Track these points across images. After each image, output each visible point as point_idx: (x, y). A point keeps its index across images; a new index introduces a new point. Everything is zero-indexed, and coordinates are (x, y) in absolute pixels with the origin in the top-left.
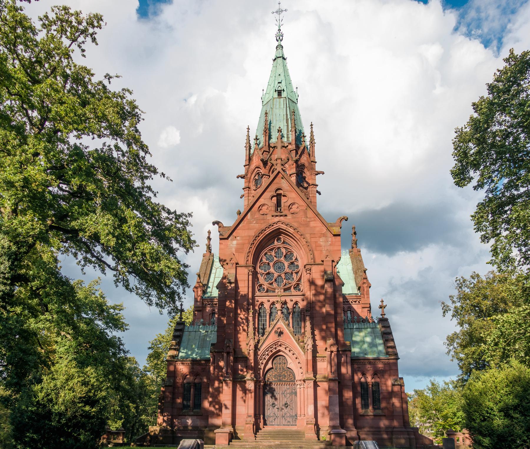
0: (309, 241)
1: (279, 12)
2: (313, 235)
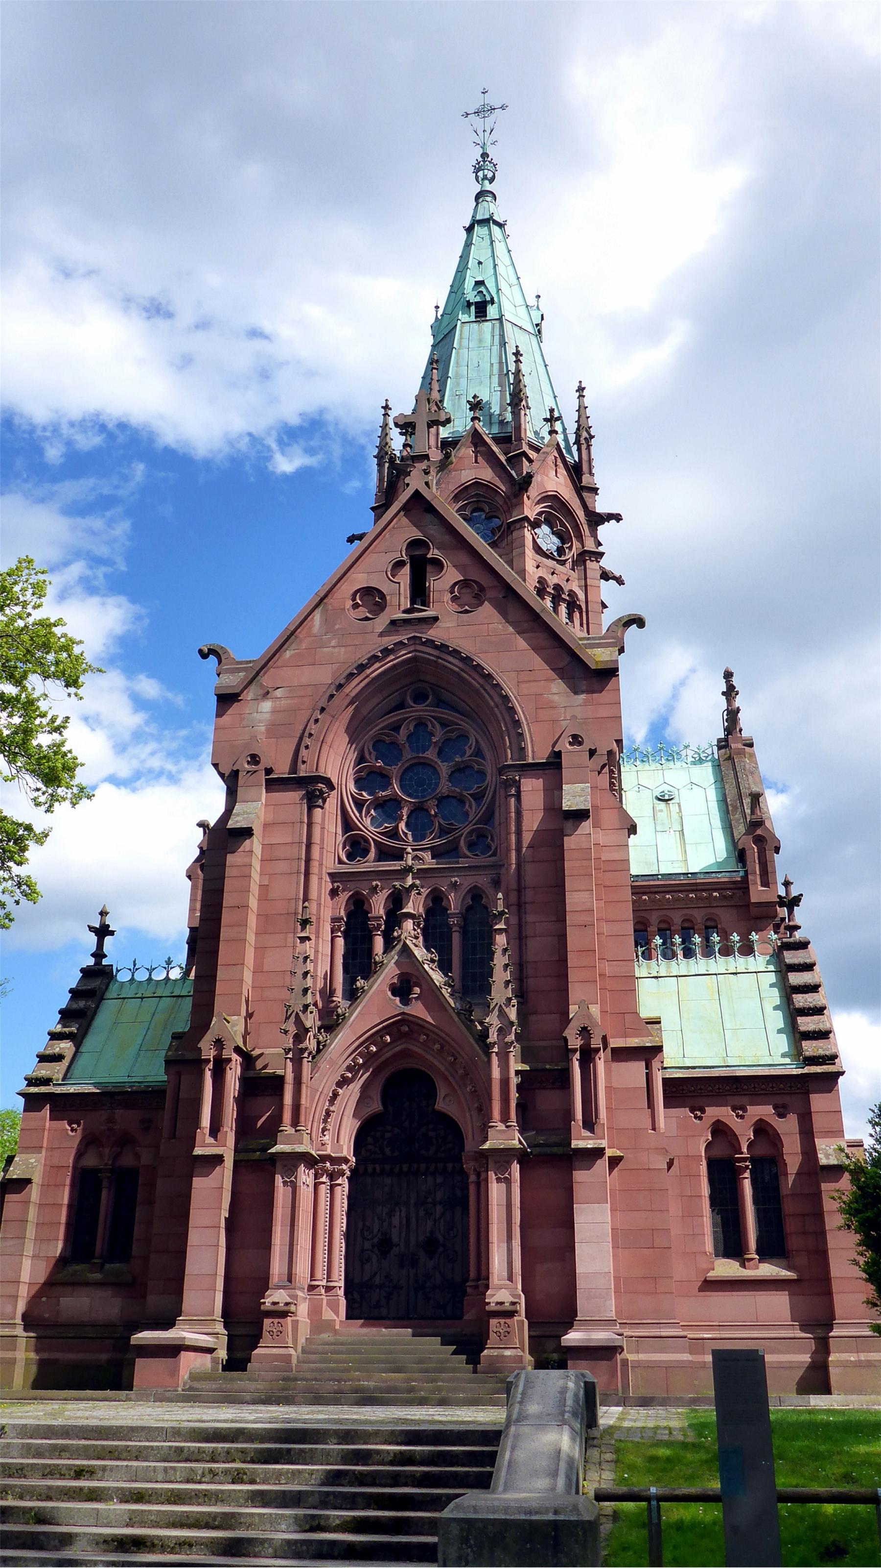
1: (484, 111)
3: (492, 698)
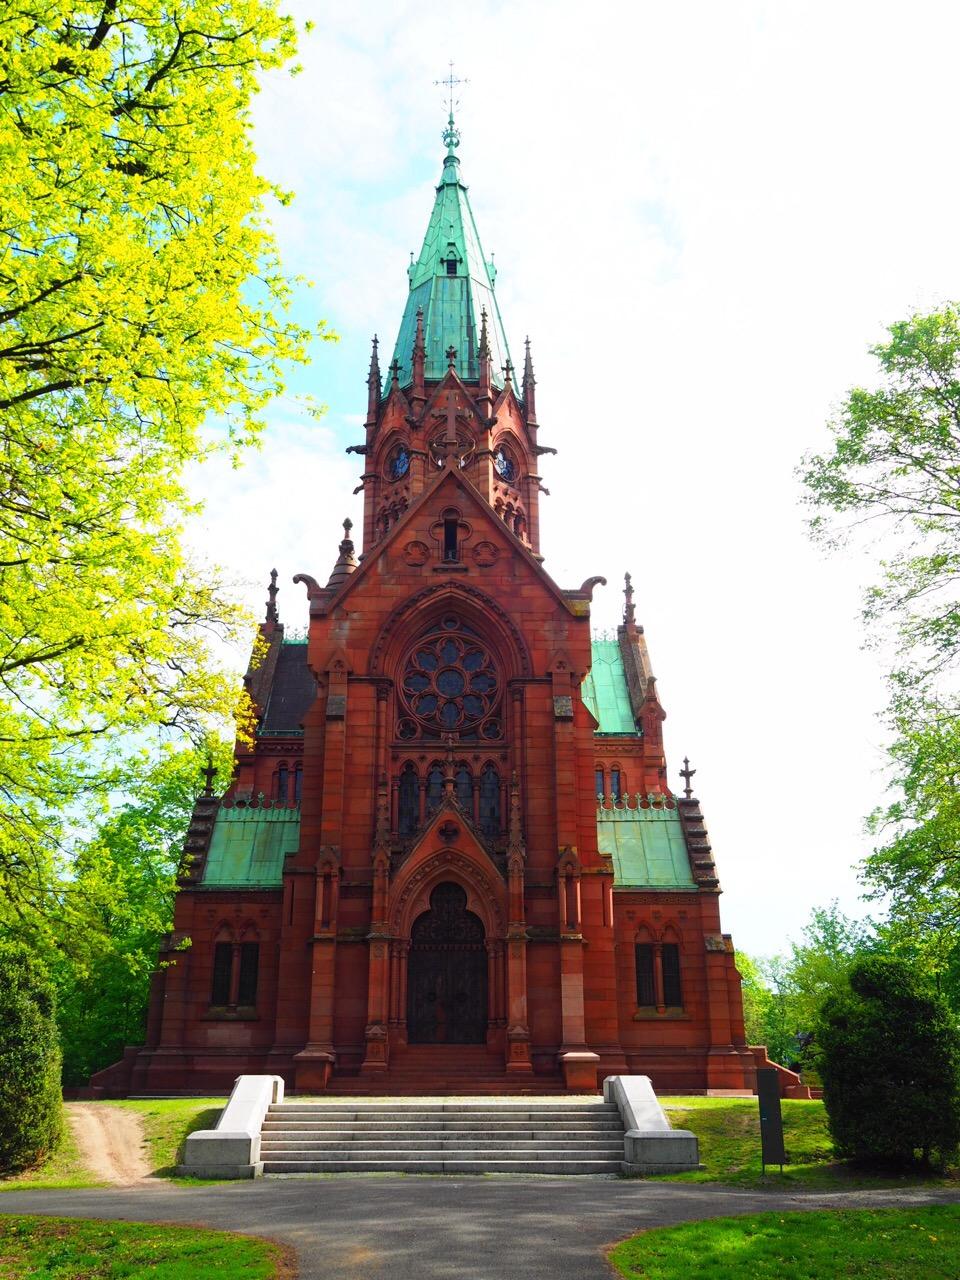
1: (451, 81)
3: (504, 630)
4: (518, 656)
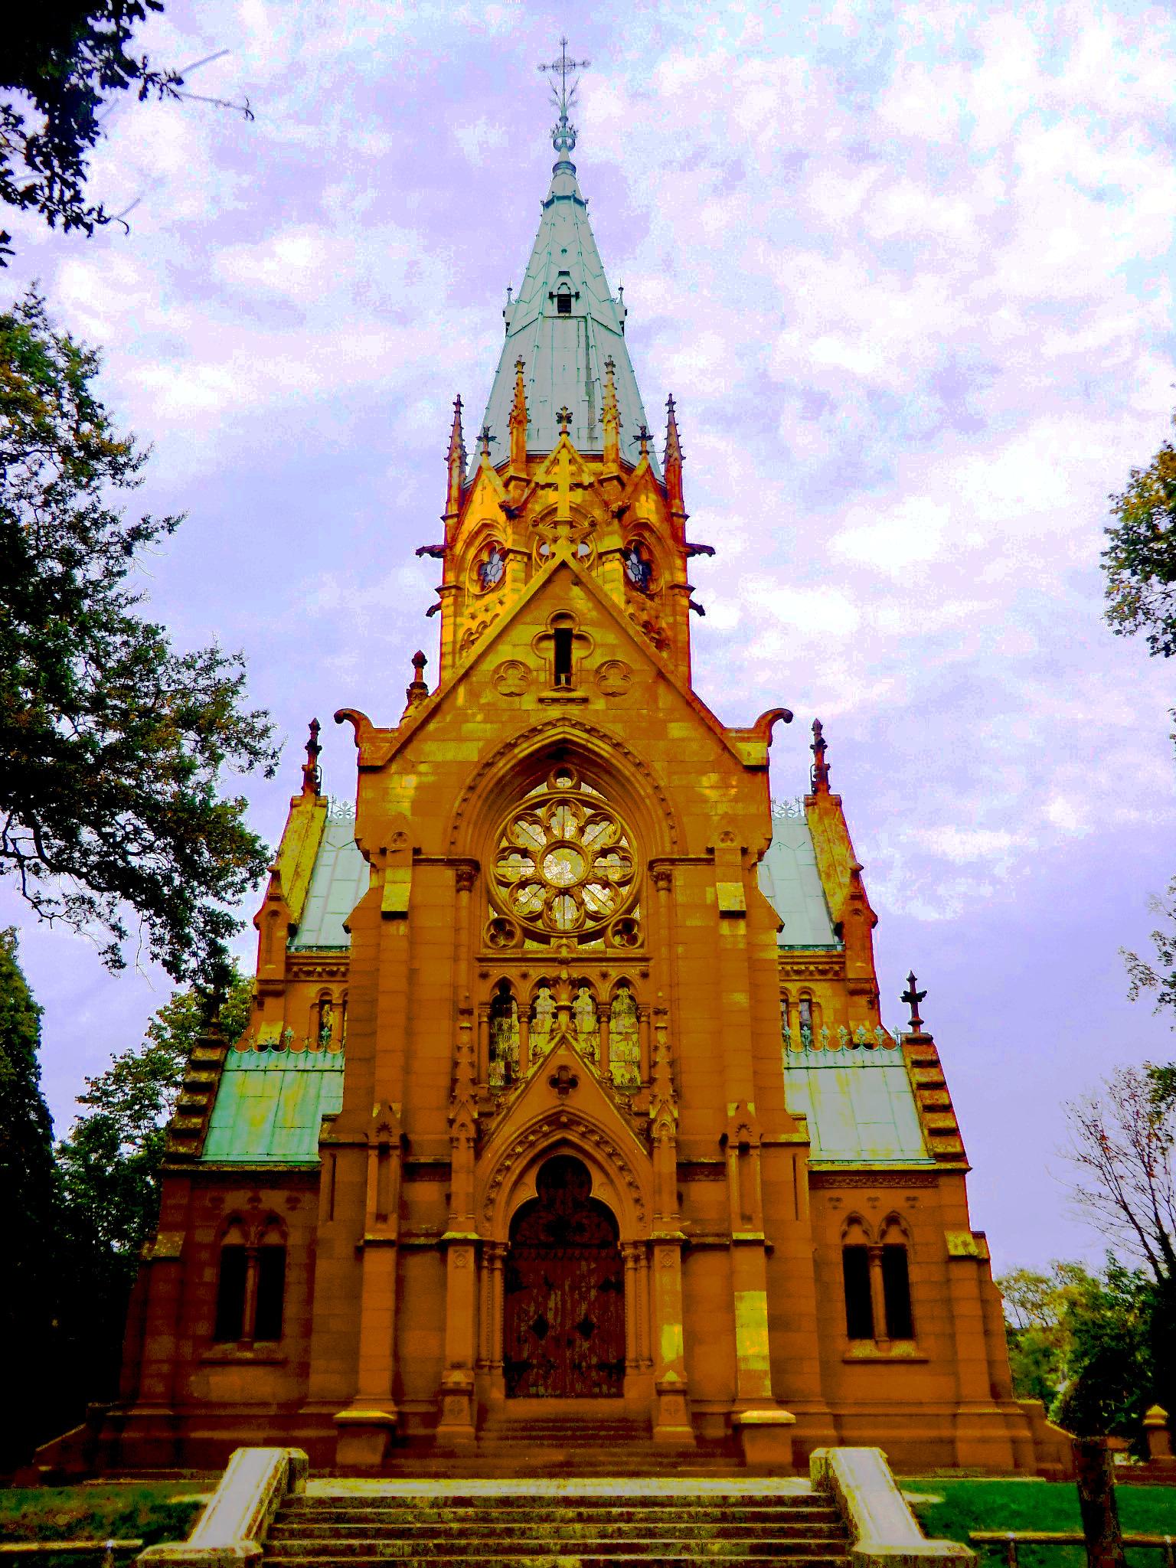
0: (662, 784)
2: (674, 761)
4: (664, 824)
